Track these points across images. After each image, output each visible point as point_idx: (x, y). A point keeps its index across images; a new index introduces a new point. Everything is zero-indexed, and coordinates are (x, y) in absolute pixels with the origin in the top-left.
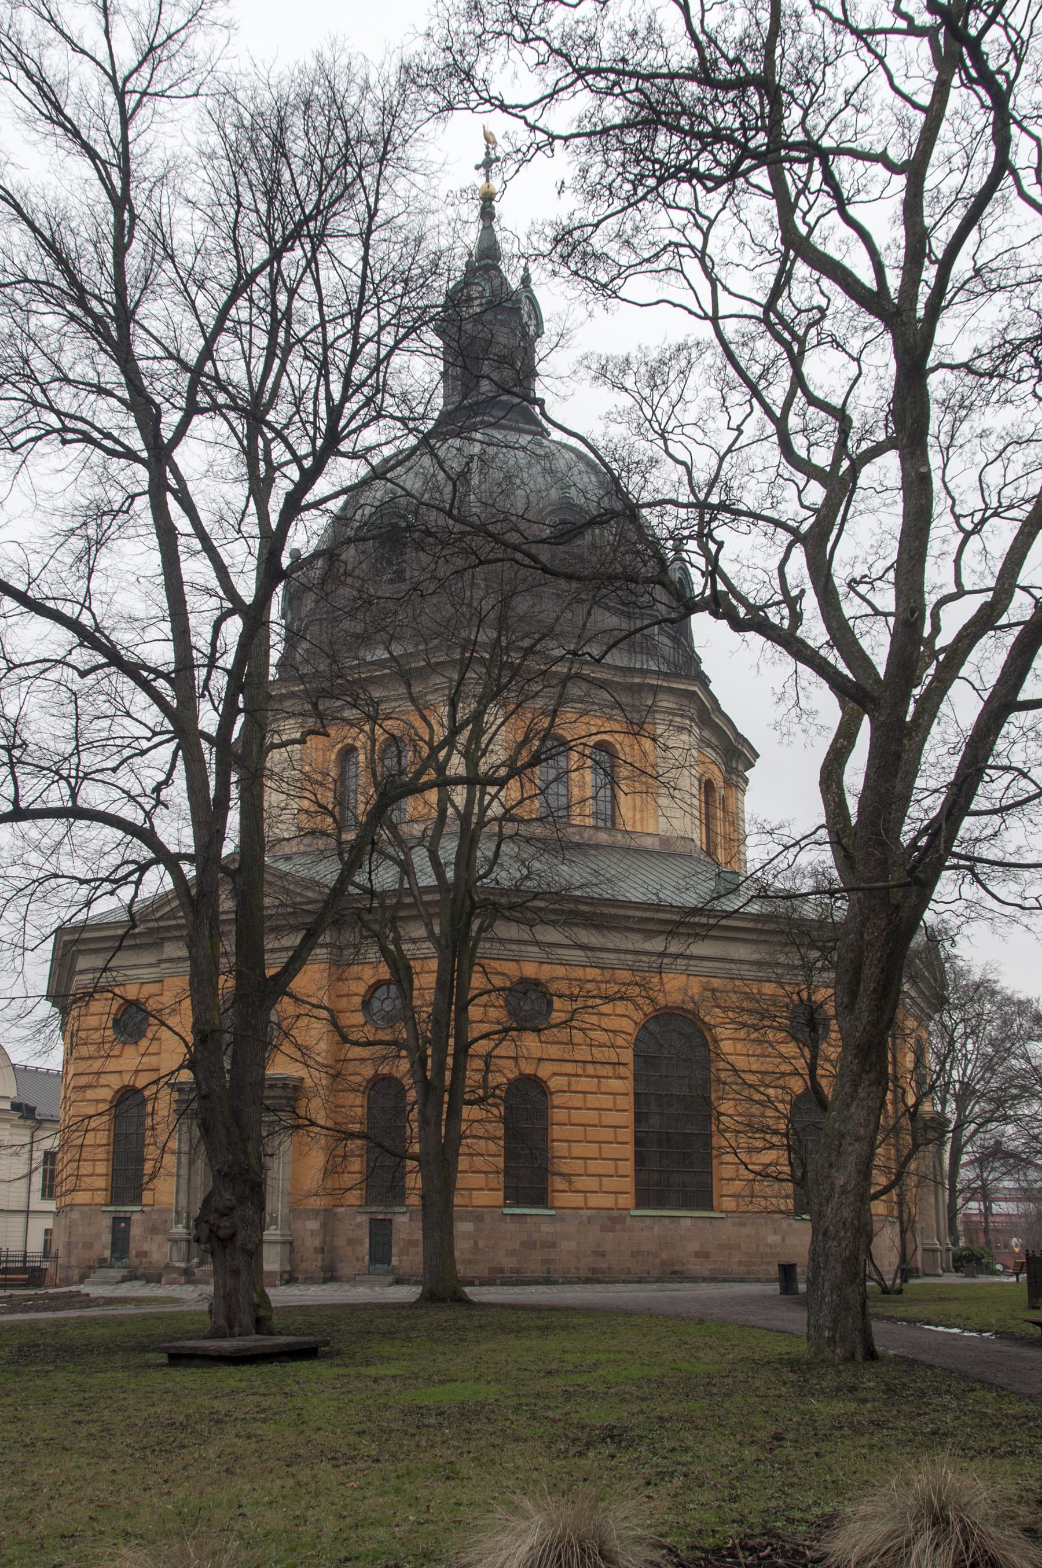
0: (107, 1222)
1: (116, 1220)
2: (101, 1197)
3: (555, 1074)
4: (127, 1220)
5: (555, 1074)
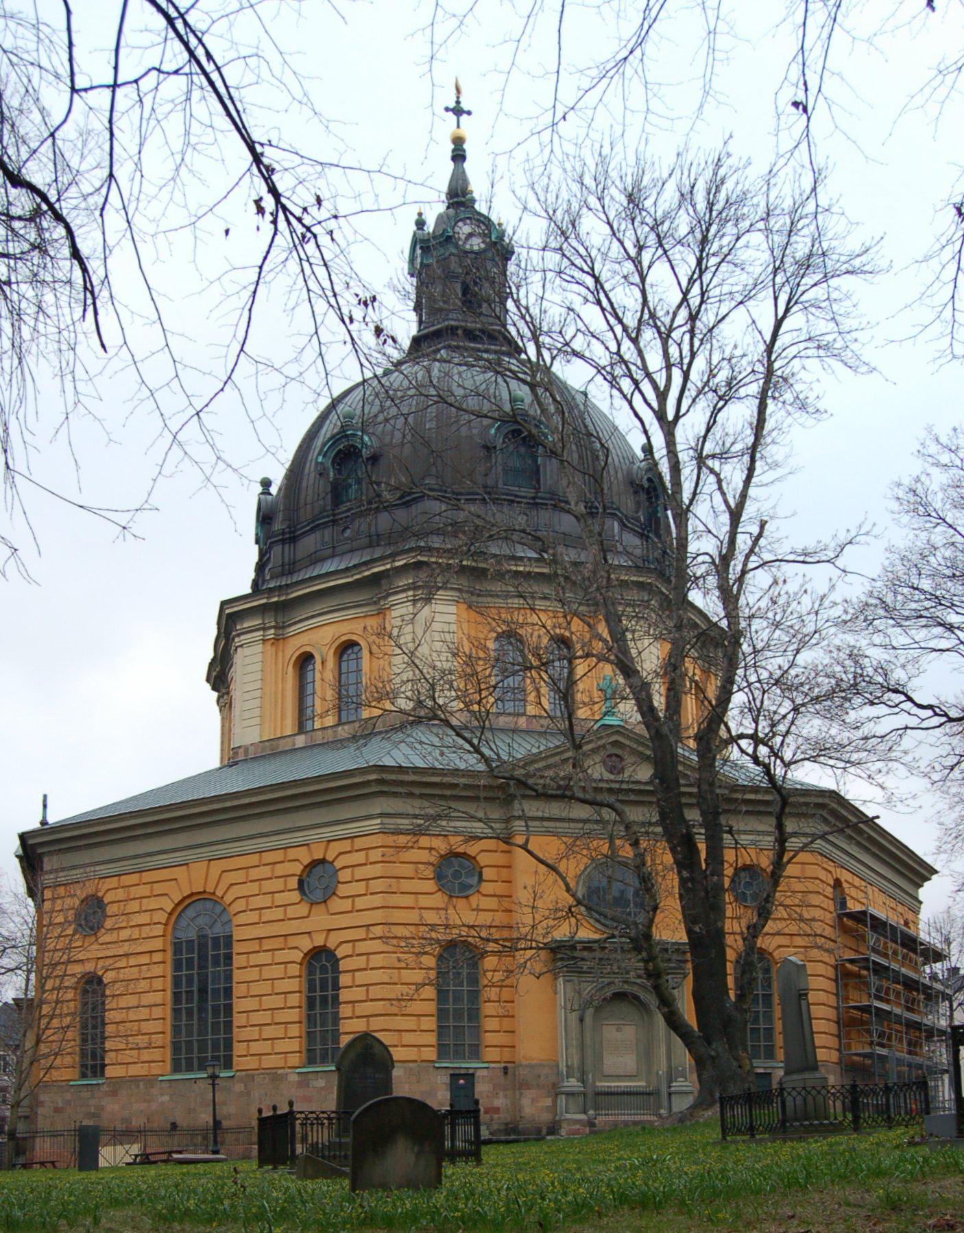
0: (444, 1079)
1: (454, 1077)
2: (430, 1054)
3: (780, 946)
4: (470, 1077)
5: (780, 946)
